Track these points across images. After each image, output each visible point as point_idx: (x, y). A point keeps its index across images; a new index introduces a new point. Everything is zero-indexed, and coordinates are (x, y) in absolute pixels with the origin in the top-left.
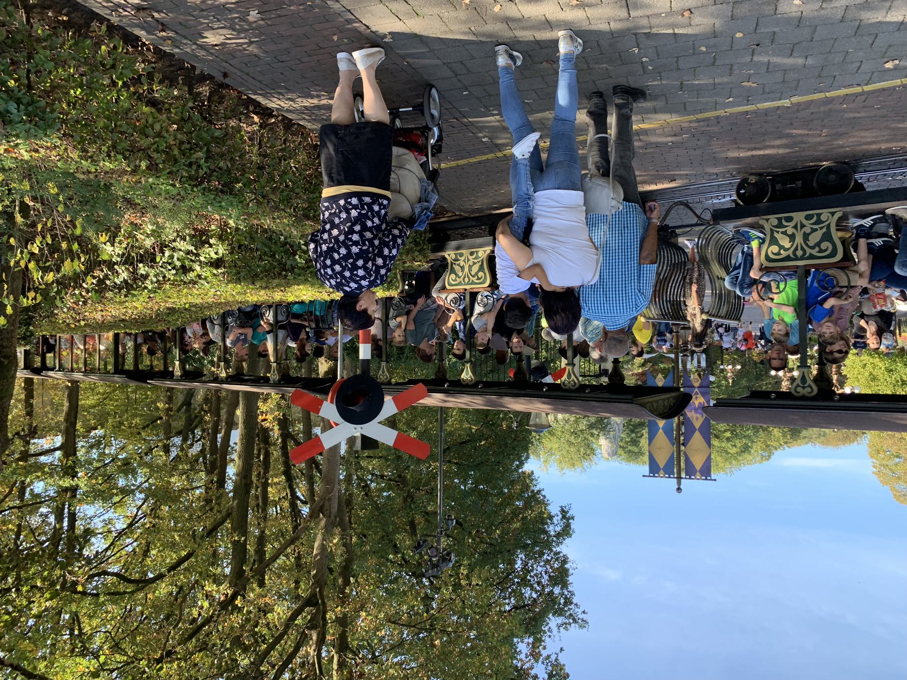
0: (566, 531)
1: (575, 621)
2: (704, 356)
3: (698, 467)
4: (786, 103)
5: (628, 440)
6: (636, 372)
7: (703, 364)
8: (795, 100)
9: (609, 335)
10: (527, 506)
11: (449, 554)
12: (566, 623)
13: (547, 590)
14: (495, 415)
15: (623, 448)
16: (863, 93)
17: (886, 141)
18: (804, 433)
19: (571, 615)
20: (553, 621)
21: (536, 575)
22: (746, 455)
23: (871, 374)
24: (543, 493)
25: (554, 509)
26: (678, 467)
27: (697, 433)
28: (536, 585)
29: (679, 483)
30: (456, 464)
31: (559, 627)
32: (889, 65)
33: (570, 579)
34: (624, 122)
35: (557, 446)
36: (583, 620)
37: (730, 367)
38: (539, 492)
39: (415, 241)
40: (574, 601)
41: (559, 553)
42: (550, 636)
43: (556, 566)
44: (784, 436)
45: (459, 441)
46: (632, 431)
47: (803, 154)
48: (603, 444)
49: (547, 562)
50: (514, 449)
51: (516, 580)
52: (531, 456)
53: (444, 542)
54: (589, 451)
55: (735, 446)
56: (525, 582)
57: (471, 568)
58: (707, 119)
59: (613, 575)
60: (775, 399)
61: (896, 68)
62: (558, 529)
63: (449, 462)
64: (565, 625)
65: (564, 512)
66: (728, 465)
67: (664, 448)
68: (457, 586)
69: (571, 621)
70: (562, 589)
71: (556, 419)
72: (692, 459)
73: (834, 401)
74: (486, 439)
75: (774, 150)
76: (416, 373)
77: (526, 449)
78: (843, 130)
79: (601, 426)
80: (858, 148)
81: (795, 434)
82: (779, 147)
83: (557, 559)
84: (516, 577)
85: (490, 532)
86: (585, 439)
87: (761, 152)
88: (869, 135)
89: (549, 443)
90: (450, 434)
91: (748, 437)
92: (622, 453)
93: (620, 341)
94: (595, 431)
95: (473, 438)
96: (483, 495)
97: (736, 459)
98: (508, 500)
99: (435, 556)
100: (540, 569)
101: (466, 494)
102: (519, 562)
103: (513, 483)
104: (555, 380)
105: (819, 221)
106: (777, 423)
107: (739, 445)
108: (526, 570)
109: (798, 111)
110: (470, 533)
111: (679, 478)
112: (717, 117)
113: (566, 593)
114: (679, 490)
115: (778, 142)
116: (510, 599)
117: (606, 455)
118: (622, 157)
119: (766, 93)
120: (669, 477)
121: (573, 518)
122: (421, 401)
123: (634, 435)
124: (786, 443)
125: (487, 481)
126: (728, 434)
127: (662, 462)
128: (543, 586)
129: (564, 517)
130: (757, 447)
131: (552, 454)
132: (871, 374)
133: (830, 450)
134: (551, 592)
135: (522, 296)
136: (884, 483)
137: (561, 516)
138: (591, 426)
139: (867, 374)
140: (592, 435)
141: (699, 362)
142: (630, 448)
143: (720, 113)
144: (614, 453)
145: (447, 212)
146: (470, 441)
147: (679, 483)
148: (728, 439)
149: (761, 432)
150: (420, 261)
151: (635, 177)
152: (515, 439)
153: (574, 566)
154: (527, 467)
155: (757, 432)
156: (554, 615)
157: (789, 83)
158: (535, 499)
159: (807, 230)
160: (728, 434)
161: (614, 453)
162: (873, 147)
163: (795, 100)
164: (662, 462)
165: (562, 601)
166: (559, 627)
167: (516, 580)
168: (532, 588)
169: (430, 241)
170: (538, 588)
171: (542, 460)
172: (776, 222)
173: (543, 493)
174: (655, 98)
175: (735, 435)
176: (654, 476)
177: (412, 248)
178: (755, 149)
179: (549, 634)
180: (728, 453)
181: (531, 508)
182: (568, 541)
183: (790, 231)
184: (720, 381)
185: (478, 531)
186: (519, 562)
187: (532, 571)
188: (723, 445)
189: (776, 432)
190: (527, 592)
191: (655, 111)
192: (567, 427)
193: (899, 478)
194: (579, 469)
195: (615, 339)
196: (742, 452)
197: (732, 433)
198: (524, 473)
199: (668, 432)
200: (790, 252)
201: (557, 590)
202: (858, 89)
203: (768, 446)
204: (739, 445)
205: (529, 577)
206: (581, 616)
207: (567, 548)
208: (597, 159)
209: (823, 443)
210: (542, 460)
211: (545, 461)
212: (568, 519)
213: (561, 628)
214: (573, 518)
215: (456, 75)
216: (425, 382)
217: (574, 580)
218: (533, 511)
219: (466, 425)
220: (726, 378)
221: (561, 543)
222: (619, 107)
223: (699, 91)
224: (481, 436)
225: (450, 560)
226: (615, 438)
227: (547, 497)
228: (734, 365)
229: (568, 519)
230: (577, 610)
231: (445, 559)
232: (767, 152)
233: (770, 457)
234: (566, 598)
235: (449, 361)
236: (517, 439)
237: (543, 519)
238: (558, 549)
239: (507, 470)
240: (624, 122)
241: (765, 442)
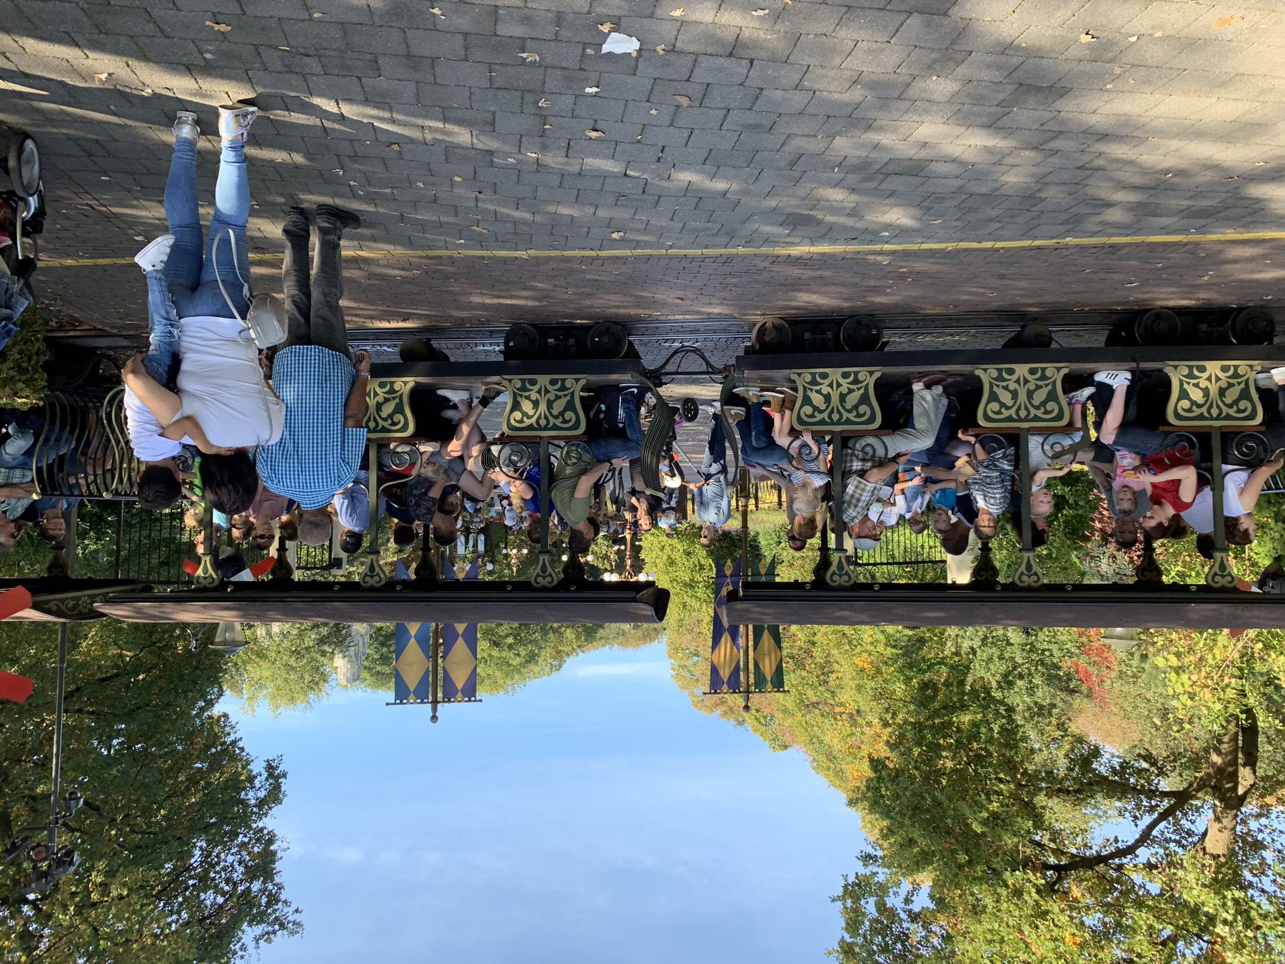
0: (274, 795)
1: (282, 926)
2: (482, 537)
3: (460, 685)
4: (523, 254)
5: (376, 657)
6: (390, 560)
7: (481, 548)
8: (532, 252)
9: (305, 516)
10: (216, 763)
11: (69, 853)
12: (267, 933)
13: (241, 889)
14: (165, 632)
15: (369, 669)
16: (598, 258)
17: (633, 307)
18: (601, 632)
19: (277, 919)
20: (249, 933)
21: (224, 869)
22: (532, 666)
23: (669, 557)
24: (241, 744)
25: (257, 767)
26: (437, 689)
27: (460, 639)
28: (223, 885)
29: (435, 710)
30: (92, 713)
31: (257, 940)
32: (615, 236)
33: (278, 866)
34: (330, 249)
35: (269, 673)
36: (294, 923)
37: (515, 551)
38: (234, 742)
39: (20, 367)
40: (283, 897)
41: (262, 830)
42: (242, 957)
43: (256, 850)
44: (578, 638)
45: (99, 676)
46: (383, 644)
47: (556, 309)
48: (340, 664)
49: (243, 845)
50: (194, 682)
51: (191, 882)
52: (228, 692)
53: (62, 839)
54: (318, 678)
55: (518, 655)
56: (205, 882)
57: (110, 873)
58: (440, 258)
59: (351, 855)
60: (339, 591)
61: (623, 240)
62: (262, 794)
63: (80, 711)
64: (267, 936)
65: (270, 768)
66: (509, 682)
67: (414, 662)
68: (85, 906)
69: (277, 927)
70: (264, 883)
71: (269, 633)
72: (453, 676)
73: (996, 591)
74: (148, 671)
75: (521, 300)
76: (21, 569)
77: (216, 681)
78: (587, 290)
79: (338, 639)
80: (608, 311)
81: (590, 635)
82: (526, 298)
83: (258, 840)
84: (191, 878)
85: (147, 812)
86: (313, 659)
87: (509, 302)
88: (616, 299)
89: (258, 670)
90: (84, 665)
91: (536, 641)
92: (368, 676)
93: (317, 525)
94: (326, 648)
95: (122, 672)
96: (142, 759)
97: (519, 672)
98: (181, 762)
99: (44, 860)
100: (230, 859)
101: (109, 762)
102: (197, 852)
103: (191, 735)
104: (255, 575)
105: (563, 388)
106: (567, 619)
107: (523, 653)
108: (209, 863)
109: (538, 265)
110: (114, 820)
111: (435, 702)
112: (451, 257)
113: (270, 886)
114: (434, 718)
115: (524, 293)
116: (179, 913)
117: (344, 682)
118: (325, 295)
119: (503, 244)
120: (422, 702)
121: (284, 775)
122: (18, 614)
123: (385, 649)
124: (579, 647)
125: (146, 737)
126: (510, 640)
127: (412, 682)
128: (235, 884)
129: (271, 775)
130: (546, 654)
131: (261, 687)
132: (669, 557)
133: (630, 652)
134: (248, 890)
135: (171, 465)
136: (684, 687)
137: (265, 775)
138: (322, 641)
139: (665, 557)
140: (323, 654)
141: (475, 546)
142: (379, 668)
143: (453, 253)
144: (355, 678)
145: (81, 323)
146: (117, 675)
147: (435, 710)
148: (510, 647)
149: (551, 635)
150: (27, 397)
151: (343, 322)
152: (196, 668)
153: (285, 845)
154: (217, 710)
155: (546, 634)
156: (250, 925)
157: (520, 236)
158: (231, 753)
159: (551, 396)
160: (510, 640)
161: (355, 678)
162: (622, 311)
163: (532, 252)
164: (412, 682)
165: (264, 900)
166: (257, 940)
167: (191, 882)
168: (218, 891)
169: (46, 367)
170: (227, 888)
171: (245, 697)
172: (519, 385)
173: (241, 744)
174: (371, 225)
175: (519, 641)
176: (401, 703)
177: (13, 377)
178: (500, 297)
179: (240, 953)
180: (509, 665)
181: (221, 767)
182: (276, 810)
183: (534, 396)
184: (502, 570)
185: (127, 816)
186: (197, 852)
187: (218, 863)
188: (504, 654)
189: (569, 634)
190: (209, 898)
191: (374, 239)
192: (286, 643)
193: (697, 680)
194: (300, 705)
195: (310, 522)
196: (527, 662)
197: (515, 638)
198: (210, 717)
199: (422, 641)
200: (533, 420)
201: (256, 886)
202: (593, 253)
203: (559, 652)
204: (523, 653)
205: (212, 875)
206: (291, 918)
207: (269, 823)
208: (294, 292)
209: (621, 644)
210: (245, 697)
211: (251, 699)
212: (278, 777)
213: (261, 942)
214: (284, 775)
215: (89, 155)
216: (26, 583)
217: (284, 869)
218: (222, 773)
219: (113, 651)
220: (509, 566)
221: (266, 814)
222: (323, 231)
223: (424, 226)
224: (138, 666)
225: (71, 863)
226: (356, 655)
227: (247, 750)
228: (520, 548)
229: (278, 777)
230: (286, 910)
231: (64, 861)
232: (514, 302)
233: (560, 666)
234: (270, 894)
235: (84, 549)
236: (204, 666)
237: (237, 784)
238: (261, 824)
239: (184, 714)
240: (330, 249)
241: (555, 647)
